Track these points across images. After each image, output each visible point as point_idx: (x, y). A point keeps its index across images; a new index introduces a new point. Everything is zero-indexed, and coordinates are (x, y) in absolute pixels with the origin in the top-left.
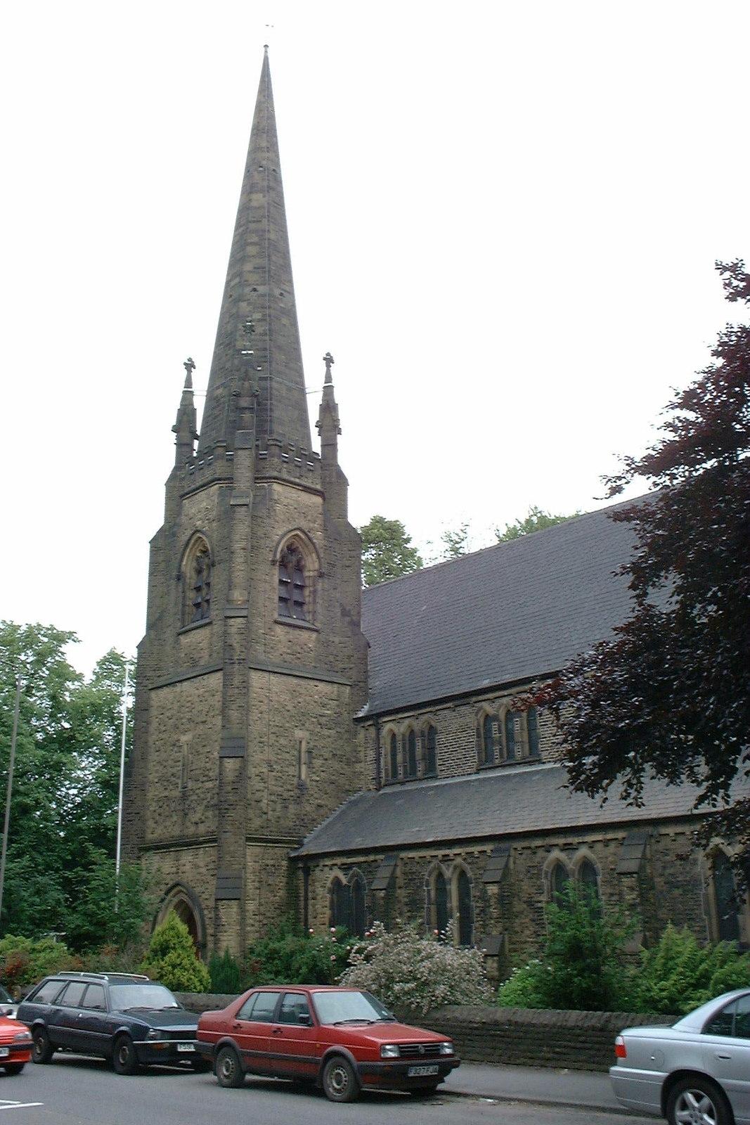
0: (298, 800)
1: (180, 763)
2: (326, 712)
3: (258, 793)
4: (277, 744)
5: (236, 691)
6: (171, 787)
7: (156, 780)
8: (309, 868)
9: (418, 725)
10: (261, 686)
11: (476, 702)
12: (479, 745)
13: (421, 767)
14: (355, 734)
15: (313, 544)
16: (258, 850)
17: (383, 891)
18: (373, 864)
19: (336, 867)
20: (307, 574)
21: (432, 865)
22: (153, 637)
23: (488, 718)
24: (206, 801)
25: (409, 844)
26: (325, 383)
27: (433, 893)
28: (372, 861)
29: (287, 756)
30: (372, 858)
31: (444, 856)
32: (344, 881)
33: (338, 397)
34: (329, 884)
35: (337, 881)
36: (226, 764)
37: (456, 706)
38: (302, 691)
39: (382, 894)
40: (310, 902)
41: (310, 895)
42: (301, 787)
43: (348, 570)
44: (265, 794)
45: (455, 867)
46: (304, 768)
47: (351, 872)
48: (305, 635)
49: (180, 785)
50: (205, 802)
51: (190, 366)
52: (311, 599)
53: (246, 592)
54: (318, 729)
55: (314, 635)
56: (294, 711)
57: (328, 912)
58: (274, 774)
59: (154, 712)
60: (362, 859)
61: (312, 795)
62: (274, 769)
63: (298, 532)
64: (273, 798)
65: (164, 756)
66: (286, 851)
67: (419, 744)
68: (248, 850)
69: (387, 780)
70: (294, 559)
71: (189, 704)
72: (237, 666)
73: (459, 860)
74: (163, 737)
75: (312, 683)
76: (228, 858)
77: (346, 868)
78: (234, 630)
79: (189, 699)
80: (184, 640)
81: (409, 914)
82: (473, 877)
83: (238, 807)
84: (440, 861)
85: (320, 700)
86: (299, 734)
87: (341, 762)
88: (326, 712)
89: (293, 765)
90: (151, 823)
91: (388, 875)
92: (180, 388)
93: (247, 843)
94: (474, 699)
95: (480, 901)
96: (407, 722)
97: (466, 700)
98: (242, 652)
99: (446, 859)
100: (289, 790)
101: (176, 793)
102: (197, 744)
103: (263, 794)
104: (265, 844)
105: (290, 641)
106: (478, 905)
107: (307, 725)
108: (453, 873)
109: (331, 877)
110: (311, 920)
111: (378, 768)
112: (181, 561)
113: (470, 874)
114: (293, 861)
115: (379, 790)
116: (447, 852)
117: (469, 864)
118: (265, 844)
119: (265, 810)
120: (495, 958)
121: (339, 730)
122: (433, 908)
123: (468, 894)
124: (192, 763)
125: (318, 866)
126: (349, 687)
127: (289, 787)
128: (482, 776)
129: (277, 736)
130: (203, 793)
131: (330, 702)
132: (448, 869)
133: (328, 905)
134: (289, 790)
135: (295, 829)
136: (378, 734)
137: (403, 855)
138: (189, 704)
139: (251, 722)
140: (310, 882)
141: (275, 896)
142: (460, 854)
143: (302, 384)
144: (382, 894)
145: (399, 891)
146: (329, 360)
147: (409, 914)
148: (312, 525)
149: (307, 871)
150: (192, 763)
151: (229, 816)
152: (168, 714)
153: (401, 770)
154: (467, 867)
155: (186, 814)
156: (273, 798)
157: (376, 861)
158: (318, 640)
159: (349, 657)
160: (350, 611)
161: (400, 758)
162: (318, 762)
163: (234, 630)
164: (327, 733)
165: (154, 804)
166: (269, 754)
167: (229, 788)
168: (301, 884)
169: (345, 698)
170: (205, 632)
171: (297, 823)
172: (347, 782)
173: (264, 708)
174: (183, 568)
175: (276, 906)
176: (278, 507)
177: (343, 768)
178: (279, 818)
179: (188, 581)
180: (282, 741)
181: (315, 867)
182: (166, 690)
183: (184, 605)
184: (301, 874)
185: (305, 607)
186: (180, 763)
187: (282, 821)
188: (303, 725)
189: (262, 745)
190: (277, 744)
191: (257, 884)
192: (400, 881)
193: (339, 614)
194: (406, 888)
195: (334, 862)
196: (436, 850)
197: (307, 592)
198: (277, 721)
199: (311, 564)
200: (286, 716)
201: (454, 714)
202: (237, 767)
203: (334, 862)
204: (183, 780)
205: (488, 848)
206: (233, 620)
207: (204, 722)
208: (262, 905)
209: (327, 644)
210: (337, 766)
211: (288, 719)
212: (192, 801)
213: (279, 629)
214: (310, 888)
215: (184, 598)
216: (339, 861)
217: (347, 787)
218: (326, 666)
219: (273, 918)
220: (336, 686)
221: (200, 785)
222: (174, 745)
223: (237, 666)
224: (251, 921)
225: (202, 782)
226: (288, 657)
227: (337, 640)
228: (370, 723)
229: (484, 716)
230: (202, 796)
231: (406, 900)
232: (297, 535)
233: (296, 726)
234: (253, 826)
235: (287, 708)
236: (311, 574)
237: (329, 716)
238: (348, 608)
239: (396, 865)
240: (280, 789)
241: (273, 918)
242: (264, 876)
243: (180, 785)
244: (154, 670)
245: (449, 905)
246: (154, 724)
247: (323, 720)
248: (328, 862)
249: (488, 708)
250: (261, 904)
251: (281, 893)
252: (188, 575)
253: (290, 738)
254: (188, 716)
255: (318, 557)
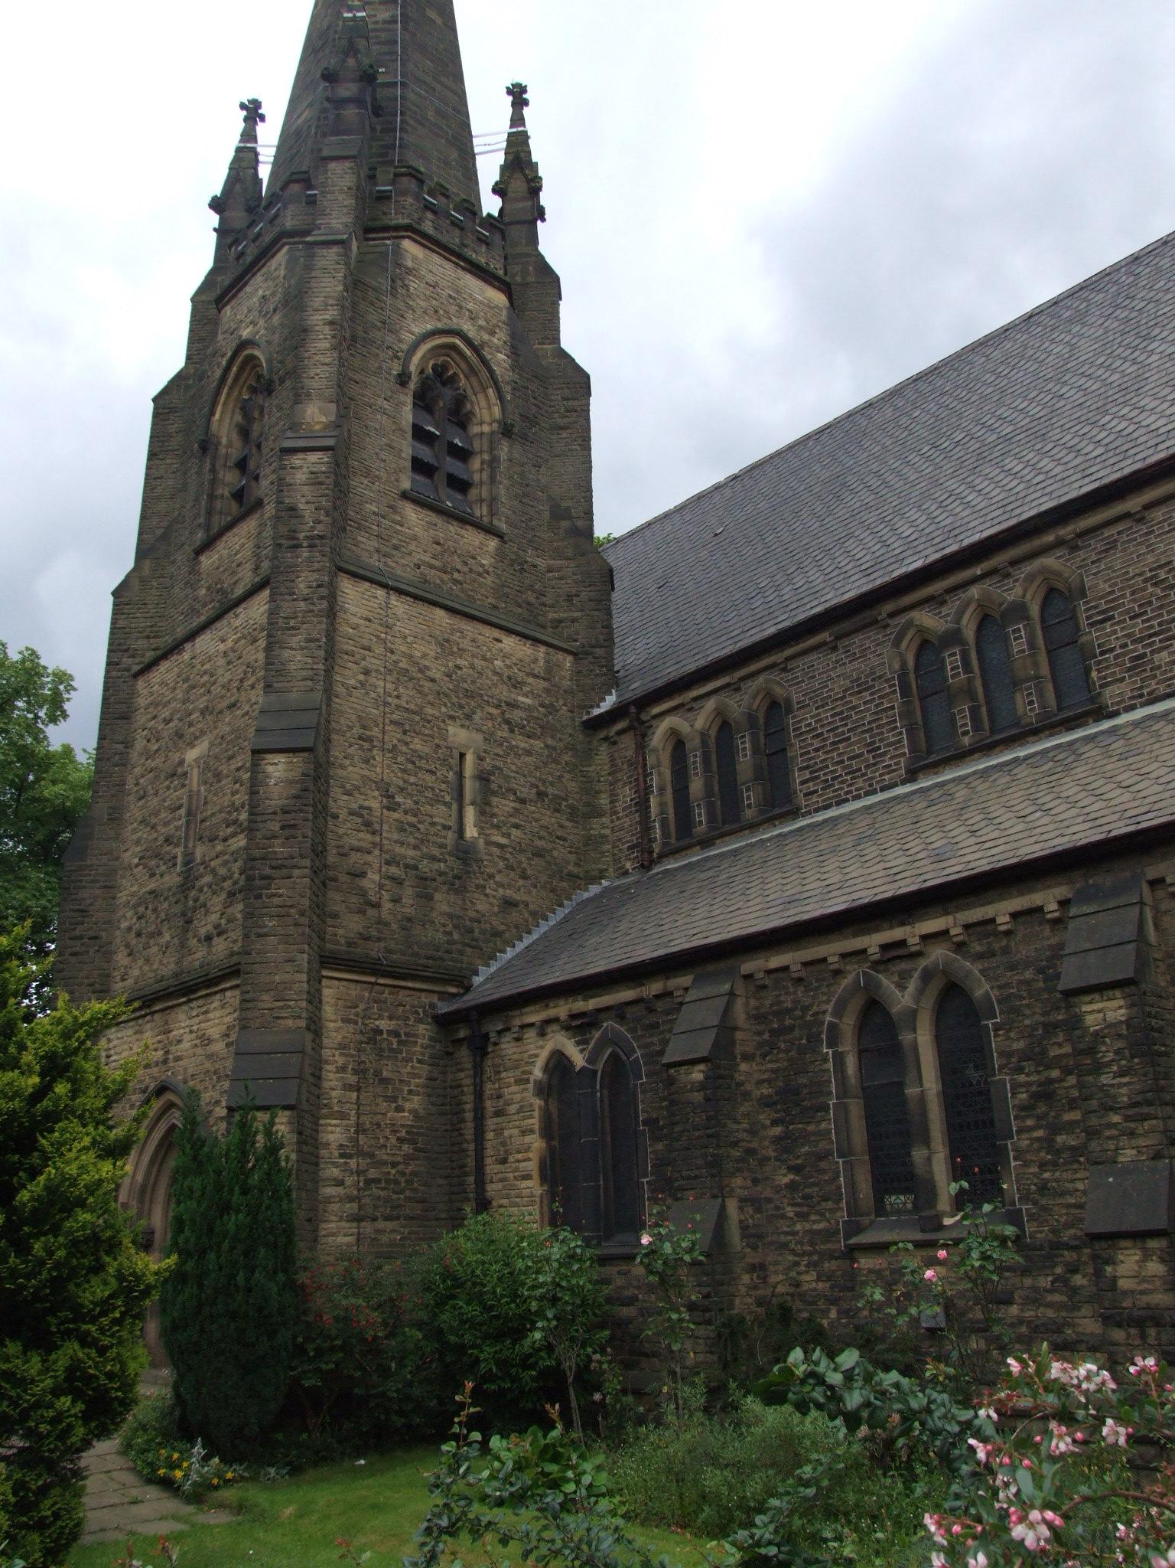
0: (458, 884)
1: (183, 811)
2: (521, 698)
3: (355, 857)
4: (404, 749)
5: (302, 605)
6: (163, 868)
7: (136, 861)
8: (486, 1036)
9: (737, 705)
10: (366, 613)
11: (892, 615)
12: (907, 714)
13: (751, 797)
14: (588, 756)
15: (491, 372)
16: (354, 991)
17: (702, 1067)
18: (660, 1006)
19: (555, 1027)
20: (475, 429)
21: (846, 982)
22: (147, 572)
23: (928, 647)
24: (229, 882)
25: (774, 932)
26: (511, 127)
27: (851, 1063)
28: (657, 997)
29: (430, 779)
30: (655, 987)
31: (885, 947)
32: (579, 1060)
33: (539, 152)
34: (538, 1073)
35: (558, 1063)
36: (270, 769)
37: (838, 638)
38: (465, 644)
39: (697, 1074)
40: (491, 1123)
41: (489, 1105)
42: (465, 853)
43: (564, 434)
44: (374, 859)
45: (927, 976)
46: (470, 814)
47: (597, 1035)
48: (471, 538)
49: (179, 860)
50: (227, 884)
51: (253, 112)
52: (485, 476)
53: (333, 407)
54: (503, 733)
55: (493, 544)
56: (447, 685)
57: (536, 1143)
58: (396, 815)
59: (141, 719)
60: (626, 995)
61: (491, 876)
62: (399, 804)
63: (457, 341)
64: (393, 870)
65: (154, 802)
66: (425, 999)
67: (745, 745)
68: (326, 992)
69: (665, 844)
70: (448, 393)
71: (206, 678)
72: (305, 554)
73: (938, 953)
74: (153, 765)
75: (491, 632)
76: (266, 1000)
77: (581, 1026)
78: (301, 477)
79: (207, 666)
80: (207, 561)
81: (777, 1130)
82: (994, 995)
83: (296, 872)
84: (876, 965)
85: (506, 673)
86: (458, 735)
87: (558, 811)
88: (521, 698)
89: (445, 804)
90: (121, 958)
91: (715, 1023)
92: (232, 140)
93: (325, 973)
94: (889, 607)
95: (1028, 1066)
96: (711, 704)
97: (868, 615)
98: (319, 522)
99: (895, 952)
100: (434, 859)
101: (173, 879)
102: (216, 757)
103: (369, 858)
104: (373, 979)
105: (438, 544)
106: (1022, 1078)
107: (477, 718)
108: (921, 992)
109: (544, 1054)
110: (491, 1168)
111: (645, 825)
112: (212, 413)
113: (982, 989)
114: (445, 1023)
115: (649, 868)
116: (897, 934)
117: (980, 957)
118: (373, 979)
119: (373, 897)
120: (1153, 1244)
121: (550, 742)
122: (856, 1110)
123: (979, 1052)
124: (206, 803)
125: (508, 1029)
126: (570, 658)
127: (436, 852)
128: (924, 783)
129: (405, 732)
130: (225, 863)
131: (531, 680)
132: (902, 987)
133: (536, 1127)
134: (434, 859)
135: (448, 952)
136: (641, 747)
137: (752, 965)
138: (206, 678)
139: (340, 689)
140: (489, 1071)
141: (399, 1109)
142: (945, 933)
143: (466, 126)
144: (697, 1074)
145: (744, 1067)
146: (518, 95)
147: (777, 1130)
148: (486, 337)
149: (481, 1047)
150: (206, 803)
151: (273, 895)
152: (166, 714)
153: (701, 815)
154: (970, 968)
155: (189, 922)
156: (393, 870)
157: (668, 994)
158: (500, 554)
159: (570, 598)
160: (568, 509)
161: (696, 786)
162: (504, 806)
163: (301, 477)
164: (523, 745)
165: (129, 914)
166: (382, 767)
167: (275, 826)
168: (466, 1078)
169: (563, 678)
170: (250, 525)
171: (456, 936)
172: (573, 858)
173: (372, 663)
174: (214, 427)
175: (403, 1134)
176: (414, 285)
177: (562, 826)
178: (410, 920)
179: (223, 451)
180: (417, 744)
181: (499, 1032)
182: (164, 666)
183: (212, 497)
184: (464, 1054)
185: (473, 493)
186: (183, 811)
187: (417, 930)
188: (468, 717)
189: (366, 745)
190: (404, 749)
191: (352, 1079)
192: (745, 1039)
193: (547, 515)
194: (764, 1056)
195: (551, 1013)
196: (855, 935)
197: (476, 463)
198: (405, 698)
199: (486, 412)
200: (426, 690)
201: (833, 657)
202: (296, 774)
203: (551, 1013)
204: (186, 847)
205: (1048, 898)
206: (301, 455)
207: (232, 706)
208: (364, 1131)
209: (522, 567)
210: (549, 819)
211: (430, 697)
212: (201, 890)
213: (412, 515)
214: (489, 1088)
215: (213, 482)
216: (562, 1009)
217: (571, 868)
218: (520, 610)
219: (394, 1165)
220: (543, 649)
221: (219, 848)
222: (173, 775)
223: (305, 554)
224: (335, 1172)
225: (225, 840)
226: (431, 574)
227: (541, 563)
228: (621, 725)
229: (917, 641)
230: (222, 871)
231: (766, 1090)
232: (454, 347)
233: (451, 717)
234: (341, 932)
235: (428, 673)
236: (486, 429)
237: (528, 708)
238: (564, 505)
239: (732, 994)
240: (411, 853)
241: (394, 1165)
242: (369, 1058)
243: (179, 860)
244: (148, 637)
245: (911, 1091)
246: (140, 744)
247: (517, 715)
248: (534, 1016)
249: (927, 619)
250: (360, 1129)
251: (416, 1103)
252: (224, 441)
253: (437, 741)
254: (202, 703)
255: (501, 397)
